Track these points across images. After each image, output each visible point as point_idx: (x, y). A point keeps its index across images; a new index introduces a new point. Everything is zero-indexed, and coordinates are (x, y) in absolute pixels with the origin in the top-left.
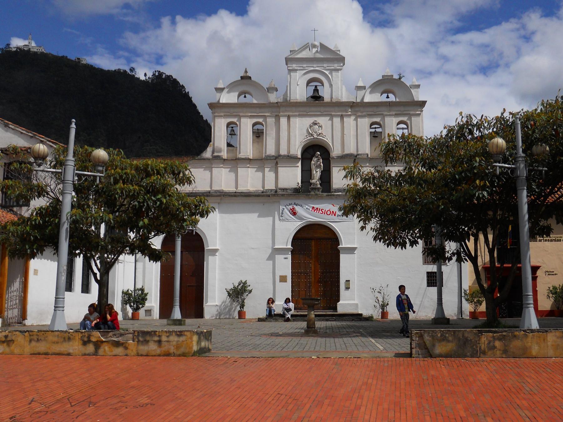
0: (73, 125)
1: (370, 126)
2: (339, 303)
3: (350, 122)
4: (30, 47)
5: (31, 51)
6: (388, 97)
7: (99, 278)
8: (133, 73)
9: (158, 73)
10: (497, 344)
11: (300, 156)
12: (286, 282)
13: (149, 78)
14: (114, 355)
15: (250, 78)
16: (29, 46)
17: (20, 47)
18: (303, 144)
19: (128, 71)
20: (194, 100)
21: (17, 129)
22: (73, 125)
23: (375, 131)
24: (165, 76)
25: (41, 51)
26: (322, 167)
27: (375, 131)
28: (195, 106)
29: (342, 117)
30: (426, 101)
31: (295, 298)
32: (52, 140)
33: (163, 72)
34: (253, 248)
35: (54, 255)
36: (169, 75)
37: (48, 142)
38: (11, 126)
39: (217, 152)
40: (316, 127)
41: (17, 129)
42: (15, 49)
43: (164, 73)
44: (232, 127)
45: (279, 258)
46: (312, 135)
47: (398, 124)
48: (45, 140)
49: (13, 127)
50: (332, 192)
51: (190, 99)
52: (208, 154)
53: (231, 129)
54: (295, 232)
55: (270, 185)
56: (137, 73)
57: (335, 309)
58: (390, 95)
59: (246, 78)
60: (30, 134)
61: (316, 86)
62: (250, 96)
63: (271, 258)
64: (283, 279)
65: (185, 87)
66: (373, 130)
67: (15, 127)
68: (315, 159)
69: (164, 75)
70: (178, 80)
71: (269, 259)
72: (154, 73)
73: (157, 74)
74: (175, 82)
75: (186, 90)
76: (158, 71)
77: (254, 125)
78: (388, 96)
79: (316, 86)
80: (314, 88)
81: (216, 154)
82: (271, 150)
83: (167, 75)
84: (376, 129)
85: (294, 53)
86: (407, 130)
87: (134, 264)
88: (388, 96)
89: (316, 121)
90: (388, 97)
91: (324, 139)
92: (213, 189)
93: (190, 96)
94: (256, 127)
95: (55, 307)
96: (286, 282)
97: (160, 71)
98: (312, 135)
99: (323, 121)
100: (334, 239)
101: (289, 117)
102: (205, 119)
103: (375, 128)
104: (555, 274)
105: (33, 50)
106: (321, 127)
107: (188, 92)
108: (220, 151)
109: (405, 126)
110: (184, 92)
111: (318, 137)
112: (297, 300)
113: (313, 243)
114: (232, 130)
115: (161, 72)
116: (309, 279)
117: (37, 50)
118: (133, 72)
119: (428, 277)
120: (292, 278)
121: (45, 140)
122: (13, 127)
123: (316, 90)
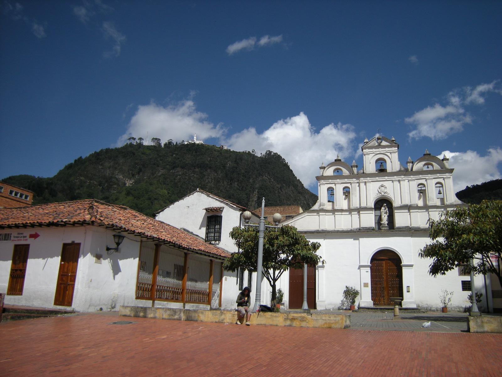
0: (264, 201)
3: (405, 184)
7: (272, 284)
8: (254, 153)
11: (373, 207)
12: (368, 287)
18: (375, 199)
19: (251, 152)
20: (291, 168)
21: (214, 197)
22: (264, 201)
26: (388, 213)
28: (292, 171)
29: (399, 181)
31: (374, 298)
34: (346, 265)
37: (231, 204)
38: (210, 196)
39: (322, 206)
40: (383, 188)
41: (214, 197)
45: (364, 270)
47: (436, 184)
48: (229, 203)
49: (212, 196)
50: (395, 229)
51: (288, 167)
52: (316, 207)
55: (356, 226)
58: (429, 166)
60: (221, 200)
61: (381, 163)
63: (359, 268)
64: (366, 285)
66: (420, 189)
67: (213, 196)
68: (383, 208)
69: (272, 153)
71: (358, 269)
74: (279, 157)
77: (344, 188)
78: (428, 166)
81: (321, 207)
82: (355, 204)
85: (366, 144)
86: (442, 188)
88: (428, 166)
89: (382, 184)
91: (388, 195)
92: (320, 228)
95: (256, 300)
96: (368, 287)
98: (381, 193)
99: (388, 184)
101: (365, 183)
102: (298, 179)
103: (421, 187)
107: (287, 163)
108: (324, 205)
109: (440, 185)
111: (385, 194)
112: (375, 299)
114: (331, 191)
116: (383, 285)
119: (462, 284)
120: (371, 285)
121: (229, 203)
122: (212, 196)
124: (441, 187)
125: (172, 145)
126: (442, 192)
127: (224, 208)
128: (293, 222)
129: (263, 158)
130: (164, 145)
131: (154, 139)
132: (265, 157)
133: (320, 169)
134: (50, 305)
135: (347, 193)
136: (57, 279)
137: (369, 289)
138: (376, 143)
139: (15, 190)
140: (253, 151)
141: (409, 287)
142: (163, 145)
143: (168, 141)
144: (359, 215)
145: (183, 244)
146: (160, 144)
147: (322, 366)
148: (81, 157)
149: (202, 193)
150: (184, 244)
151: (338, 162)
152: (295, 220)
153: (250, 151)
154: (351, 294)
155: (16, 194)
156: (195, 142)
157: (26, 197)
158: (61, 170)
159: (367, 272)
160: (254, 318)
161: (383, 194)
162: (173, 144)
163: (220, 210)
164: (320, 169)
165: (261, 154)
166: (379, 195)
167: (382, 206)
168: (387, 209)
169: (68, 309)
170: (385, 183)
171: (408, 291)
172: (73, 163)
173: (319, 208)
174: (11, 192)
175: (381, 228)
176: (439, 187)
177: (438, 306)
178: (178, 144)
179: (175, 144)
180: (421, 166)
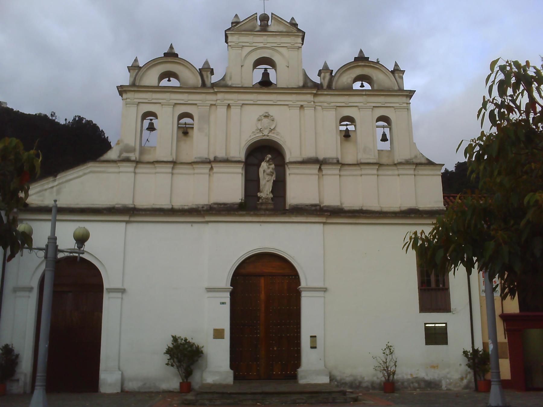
1: (340, 122)
6: (362, 86)
8: (54, 118)
9: (78, 118)
12: (223, 338)
13: (69, 122)
15: (176, 55)
19: (49, 115)
23: (347, 128)
24: (86, 121)
27: (347, 128)
30: (415, 91)
35: (389, 347)
36: (89, 120)
40: (265, 120)
43: (84, 118)
44: (151, 120)
46: (260, 131)
53: (149, 121)
54: (238, 264)
56: (57, 117)
57: (294, 377)
59: (171, 55)
62: (177, 81)
64: (218, 334)
65: (105, 132)
69: (84, 120)
70: (98, 125)
73: (77, 119)
75: (105, 135)
76: (78, 116)
78: (362, 84)
79: (266, 69)
80: (263, 71)
83: (88, 120)
84: (348, 127)
88: (362, 84)
90: (362, 86)
93: (109, 141)
94: (183, 121)
96: (223, 338)
97: (80, 116)
100: (292, 276)
103: (347, 125)
107: (108, 137)
110: (103, 137)
113: (262, 281)
118: (53, 117)
123: (266, 74)
124: (386, 127)
126: (388, 137)
128: (57, 185)
129: (68, 126)
133: (221, 304)
136: (518, 307)
137: (225, 343)
140: (51, 114)
141: (315, 337)
151: (170, 59)
152: (61, 181)
159: (223, 303)
161: (266, 132)
164: (221, 304)
167: (262, 160)
170: (273, 111)
171: (313, 347)
173: (119, 157)
175: (259, 207)
176: (384, 127)
177: (375, 379)
180: (349, 82)
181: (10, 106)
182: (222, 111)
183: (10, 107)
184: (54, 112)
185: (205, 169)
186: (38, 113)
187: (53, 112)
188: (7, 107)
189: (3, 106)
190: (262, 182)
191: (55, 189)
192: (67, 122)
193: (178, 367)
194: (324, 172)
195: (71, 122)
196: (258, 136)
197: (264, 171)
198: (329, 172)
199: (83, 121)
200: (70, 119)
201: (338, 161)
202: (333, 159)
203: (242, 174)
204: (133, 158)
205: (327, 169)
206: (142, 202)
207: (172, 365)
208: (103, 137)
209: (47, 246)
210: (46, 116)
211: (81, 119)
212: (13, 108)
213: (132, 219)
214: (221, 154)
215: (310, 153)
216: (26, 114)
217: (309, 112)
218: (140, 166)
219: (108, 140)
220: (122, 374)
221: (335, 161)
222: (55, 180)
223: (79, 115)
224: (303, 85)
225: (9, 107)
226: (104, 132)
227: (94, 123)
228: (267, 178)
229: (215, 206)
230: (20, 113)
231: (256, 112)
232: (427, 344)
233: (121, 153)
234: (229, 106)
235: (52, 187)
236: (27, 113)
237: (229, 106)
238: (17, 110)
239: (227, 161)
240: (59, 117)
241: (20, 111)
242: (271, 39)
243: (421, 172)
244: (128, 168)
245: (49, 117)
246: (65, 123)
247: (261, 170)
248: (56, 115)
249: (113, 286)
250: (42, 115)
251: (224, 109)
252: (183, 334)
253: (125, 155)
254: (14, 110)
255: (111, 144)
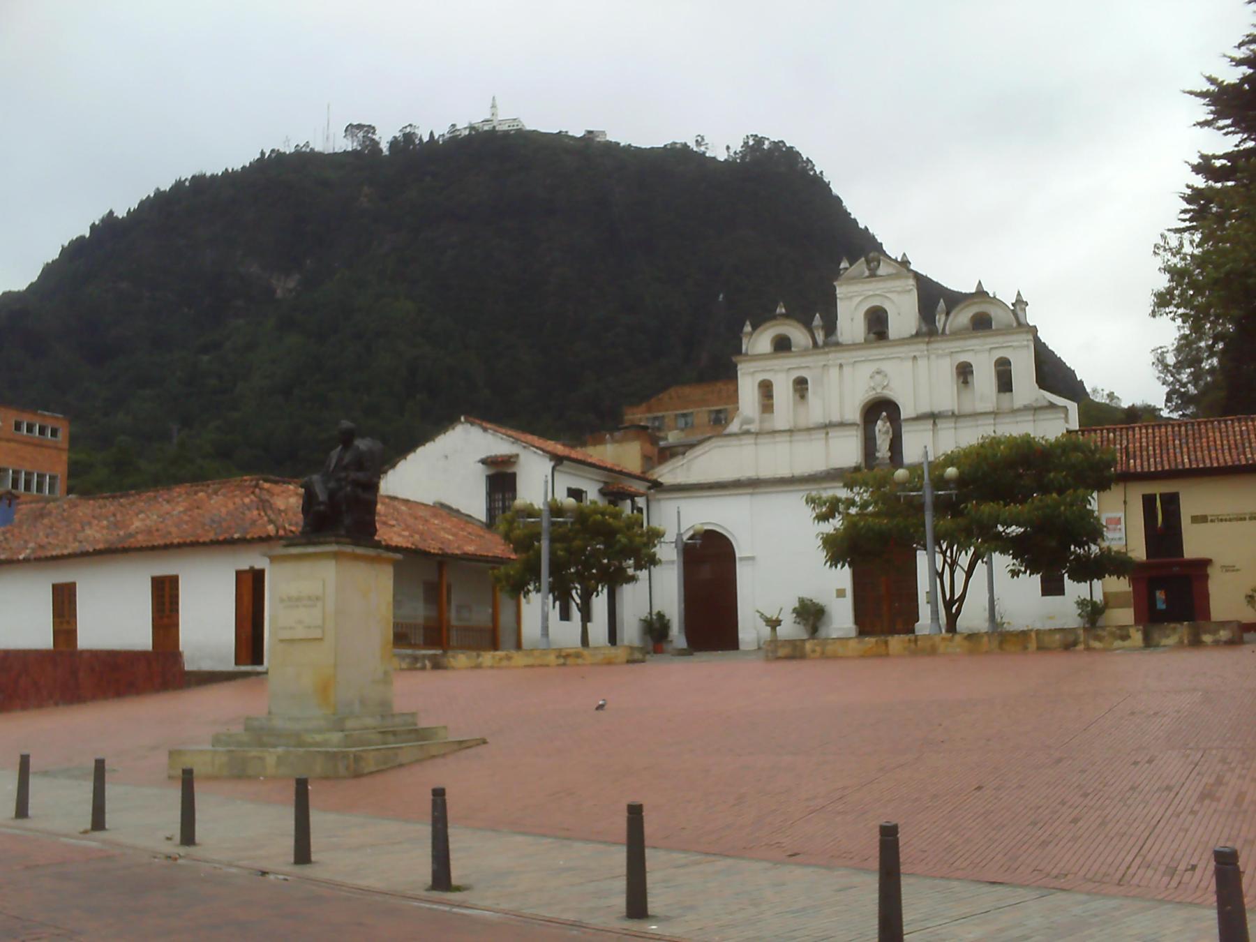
2: (918, 623)
4: (495, 123)
5: (497, 131)
8: (703, 149)
9: (754, 140)
10: (818, 649)
12: (844, 596)
13: (735, 153)
14: (999, 888)
16: (491, 121)
17: (476, 125)
24: (770, 143)
25: (515, 128)
32: (447, 909)
33: (764, 136)
36: (776, 140)
40: (878, 377)
42: (467, 132)
43: (765, 138)
52: (734, 427)
56: (709, 146)
64: (841, 593)
65: (814, 162)
68: (879, 423)
69: (767, 142)
70: (798, 149)
72: (746, 141)
75: (815, 168)
76: (752, 135)
83: (774, 142)
87: (648, 582)
96: (844, 596)
97: (756, 136)
104: (1238, 570)
105: (501, 129)
106: (886, 376)
107: (821, 173)
115: (760, 136)
117: (509, 126)
125: (417, 142)
127: (517, 456)
130: (391, 147)
131: (352, 129)
132: (743, 158)
134: (230, 666)
135: (801, 385)
137: (848, 601)
138: (866, 270)
139: (26, 419)
140: (697, 141)
142: (384, 147)
143: (401, 131)
144: (827, 439)
145: (432, 546)
146: (375, 144)
147: (1076, 874)
148: (111, 213)
149: (472, 424)
150: (434, 548)
153: (689, 144)
154: (811, 614)
155: (30, 429)
156: (494, 127)
157: (54, 433)
158: (47, 264)
160: (1147, 765)
161: (879, 390)
162: (421, 139)
163: (509, 461)
165: (728, 148)
166: (871, 393)
168: (888, 424)
169: (259, 668)
170: (887, 366)
172: (87, 235)
173: (740, 428)
174: (18, 427)
178: (436, 137)
179: (426, 138)
181: (612, 137)
182: (834, 372)
183: (613, 140)
184: (702, 135)
185: (821, 435)
186: (670, 142)
187: (699, 136)
188: (608, 141)
189: (598, 139)
190: (879, 442)
191: (685, 466)
192: (732, 154)
193: (805, 625)
194: (939, 426)
195: (740, 152)
196: (871, 395)
197: (879, 431)
198: (944, 426)
199: (764, 144)
200: (737, 146)
201: (953, 413)
202: (947, 411)
203: (857, 436)
204: (753, 430)
205: (941, 424)
206: (765, 473)
207: (799, 623)
208: (812, 173)
209: (676, 540)
210: (685, 146)
211: (759, 141)
212: (618, 141)
213: (757, 490)
214: (836, 418)
215: (925, 409)
216: (645, 149)
217: (922, 363)
218: (759, 436)
219: (822, 178)
220: (758, 634)
221: (950, 413)
222: (684, 458)
223: (754, 134)
224: (917, 332)
225: (610, 139)
226: (811, 162)
227: (788, 145)
228: (883, 437)
229: (832, 471)
230: (633, 149)
231: (866, 370)
232: (1043, 595)
233: (742, 425)
234: (841, 366)
235: (683, 465)
236: (648, 147)
237: (841, 366)
238: (628, 143)
239: (842, 425)
240: (713, 144)
241: (634, 145)
242: (881, 285)
243: (1042, 417)
244: (749, 440)
245: (692, 149)
246: (726, 157)
247: (877, 429)
248: (706, 141)
249: (744, 555)
250: (678, 146)
251: (837, 369)
252: (807, 595)
253: (745, 427)
254: (622, 144)
255: (831, 186)
